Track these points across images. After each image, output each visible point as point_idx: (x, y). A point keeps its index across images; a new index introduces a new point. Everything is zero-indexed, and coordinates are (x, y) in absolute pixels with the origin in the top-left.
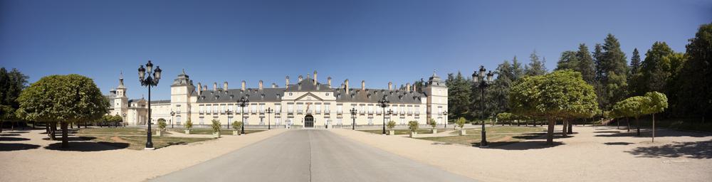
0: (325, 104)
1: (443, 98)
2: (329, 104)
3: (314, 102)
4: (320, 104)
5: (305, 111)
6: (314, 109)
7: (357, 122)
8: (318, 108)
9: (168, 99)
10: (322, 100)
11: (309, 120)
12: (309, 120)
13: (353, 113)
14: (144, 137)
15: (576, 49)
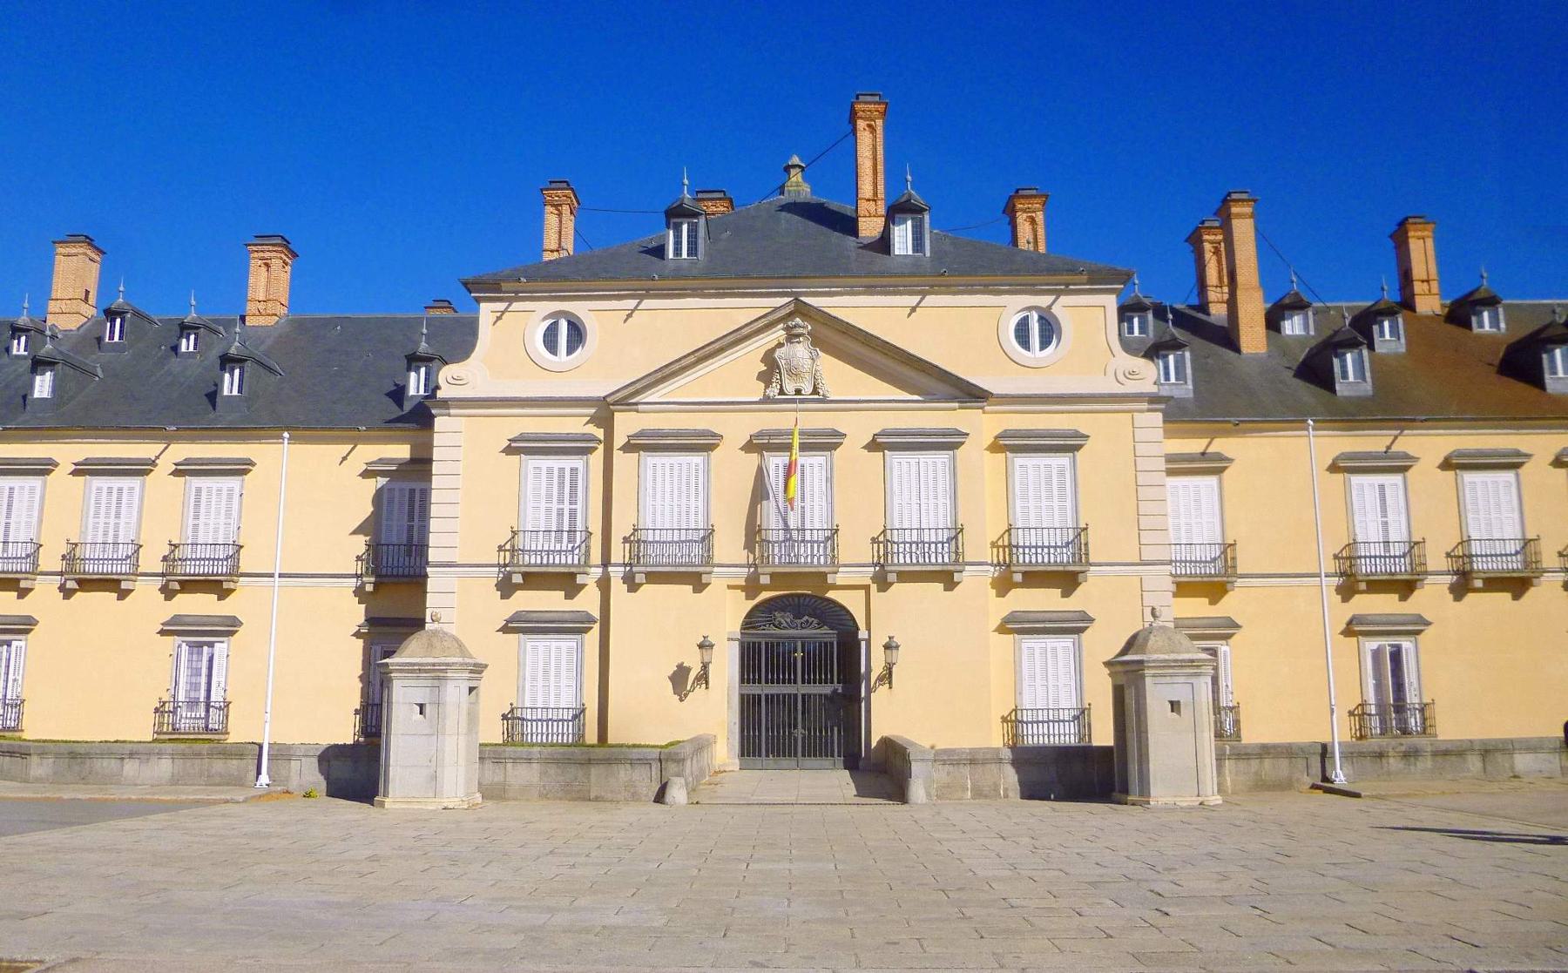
0: (1010, 444)
1: (1518, 527)
2: (1068, 444)
3: (858, 428)
4: (948, 442)
5: (730, 548)
6: (857, 502)
7: (1433, 673)
8: (917, 495)
9: (425, 456)
10: (971, 395)
11: (806, 678)
12: (806, 678)
13: (1373, 583)
14: (535, 648)
15: (1107, 671)
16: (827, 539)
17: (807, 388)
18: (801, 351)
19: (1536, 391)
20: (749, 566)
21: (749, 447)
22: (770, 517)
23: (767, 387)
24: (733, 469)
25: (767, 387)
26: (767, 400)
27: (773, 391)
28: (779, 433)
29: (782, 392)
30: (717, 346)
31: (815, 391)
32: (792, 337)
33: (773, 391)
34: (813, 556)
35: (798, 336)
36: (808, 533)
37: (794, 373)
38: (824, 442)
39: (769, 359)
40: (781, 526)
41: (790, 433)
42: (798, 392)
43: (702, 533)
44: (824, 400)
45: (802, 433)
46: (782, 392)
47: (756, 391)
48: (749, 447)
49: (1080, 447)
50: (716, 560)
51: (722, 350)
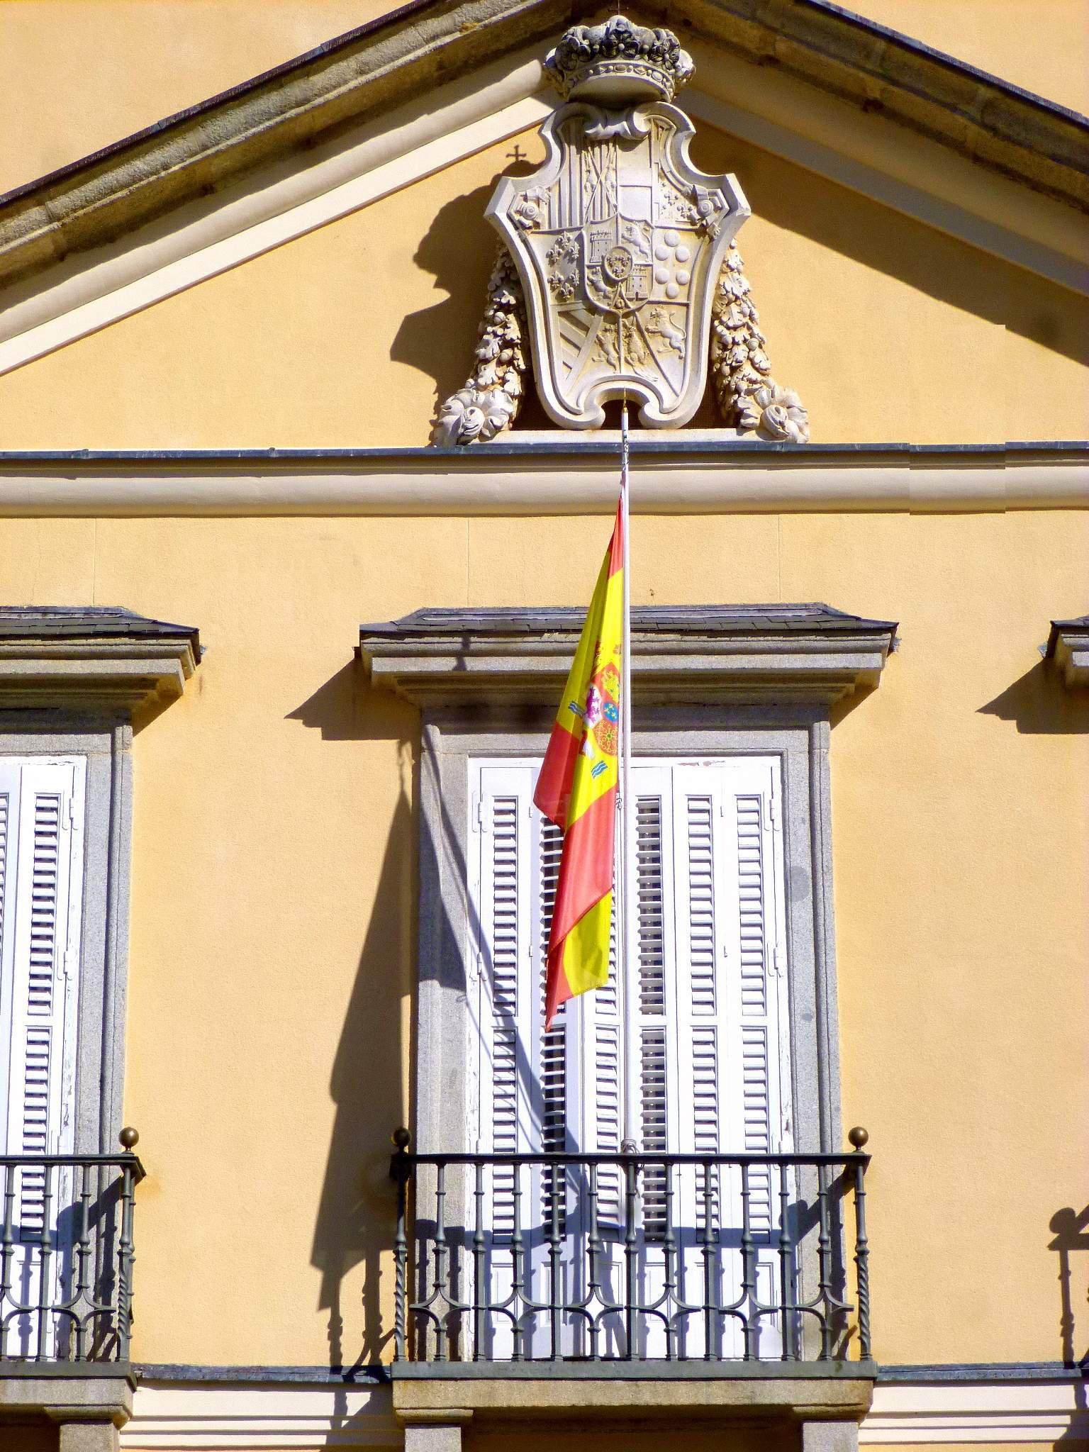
16: (801, 1218)
17: (674, 393)
18: (642, 189)
19: (298, 704)
20: (340, 1379)
21: (356, 702)
22: (463, 1091)
23: (448, 387)
24: (256, 824)
25: (448, 387)
26: (453, 450)
27: (489, 404)
28: (508, 628)
29: (532, 412)
30: (172, 158)
31: (718, 406)
32: (584, 116)
33: (489, 404)
34: (715, 1313)
35: (626, 102)
36: (685, 1179)
37: (602, 306)
38: (771, 682)
39: (470, 253)
40: (530, 1138)
41: (578, 626)
42: (624, 408)
43: (65, 1188)
44: (776, 450)
45: (647, 624)
46: (532, 412)
47: (401, 407)
48: (356, 702)
49: (855, 688)
50: (147, 1344)
51: (196, 194)
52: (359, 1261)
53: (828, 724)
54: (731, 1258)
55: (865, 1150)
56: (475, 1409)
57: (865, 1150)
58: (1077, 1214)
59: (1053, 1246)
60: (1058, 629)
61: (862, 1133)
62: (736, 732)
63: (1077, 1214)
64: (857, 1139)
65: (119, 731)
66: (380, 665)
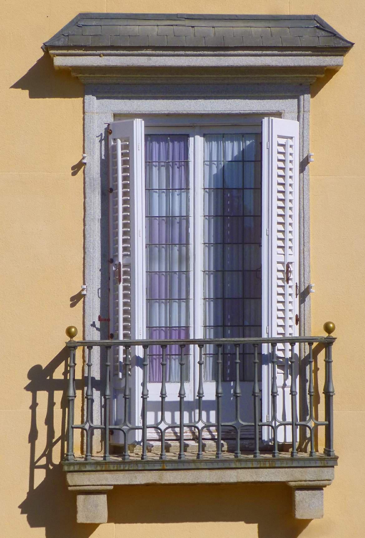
19: (13, 84)
52: (149, 402)
53: (310, 95)
54: (190, 397)
55: (333, 335)
56: (115, 486)
57: (333, 335)
58: (43, 368)
59: (27, 388)
60: (47, 48)
61: (331, 325)
62: (255, 101)
63: (43, 368)
64: (328, 329)
65: (302, 97)
66: (59, 61)
